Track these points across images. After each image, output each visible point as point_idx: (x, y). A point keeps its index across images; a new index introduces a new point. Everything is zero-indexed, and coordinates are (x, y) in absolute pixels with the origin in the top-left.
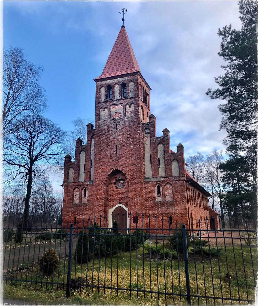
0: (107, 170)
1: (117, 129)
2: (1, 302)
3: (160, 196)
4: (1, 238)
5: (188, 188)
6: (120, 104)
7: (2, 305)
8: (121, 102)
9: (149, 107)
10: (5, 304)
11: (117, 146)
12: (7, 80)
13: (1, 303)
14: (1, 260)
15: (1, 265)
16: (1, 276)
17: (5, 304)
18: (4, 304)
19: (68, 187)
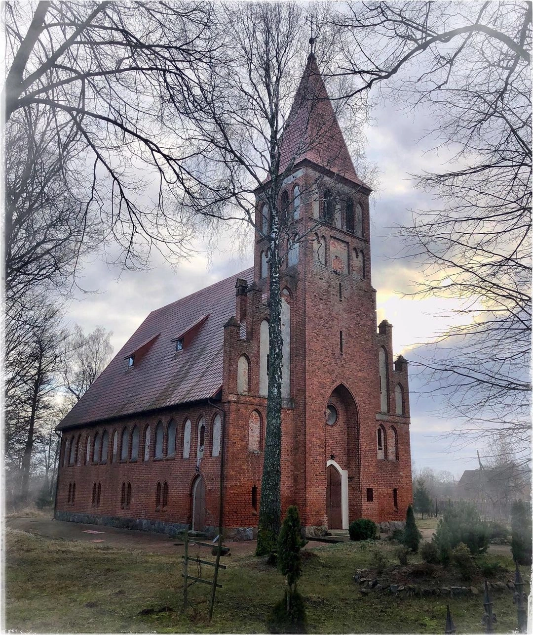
0: (327, 382)
1: (341, 297)
2: (2, 626)
3: (381, 449)
4: (2, 494)
5: (147, 450)
6: (343, 242)
7: (4, 632)
8: (346, 240)
9: (7, 30)
10: (11, 632)
11: (341, 332)
12: (69, 172)
13: (2, 629)
14: (2, 540)
15: (1, 550)
16: (2, 574)
17: (9, 631)
18: (7, 631)
19: (240, 405)
